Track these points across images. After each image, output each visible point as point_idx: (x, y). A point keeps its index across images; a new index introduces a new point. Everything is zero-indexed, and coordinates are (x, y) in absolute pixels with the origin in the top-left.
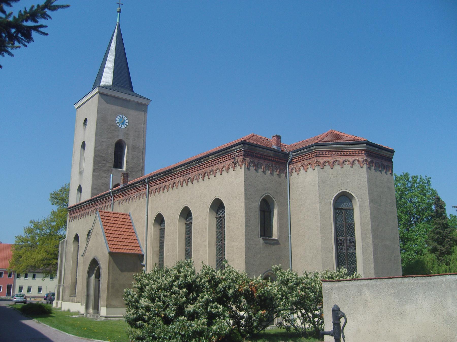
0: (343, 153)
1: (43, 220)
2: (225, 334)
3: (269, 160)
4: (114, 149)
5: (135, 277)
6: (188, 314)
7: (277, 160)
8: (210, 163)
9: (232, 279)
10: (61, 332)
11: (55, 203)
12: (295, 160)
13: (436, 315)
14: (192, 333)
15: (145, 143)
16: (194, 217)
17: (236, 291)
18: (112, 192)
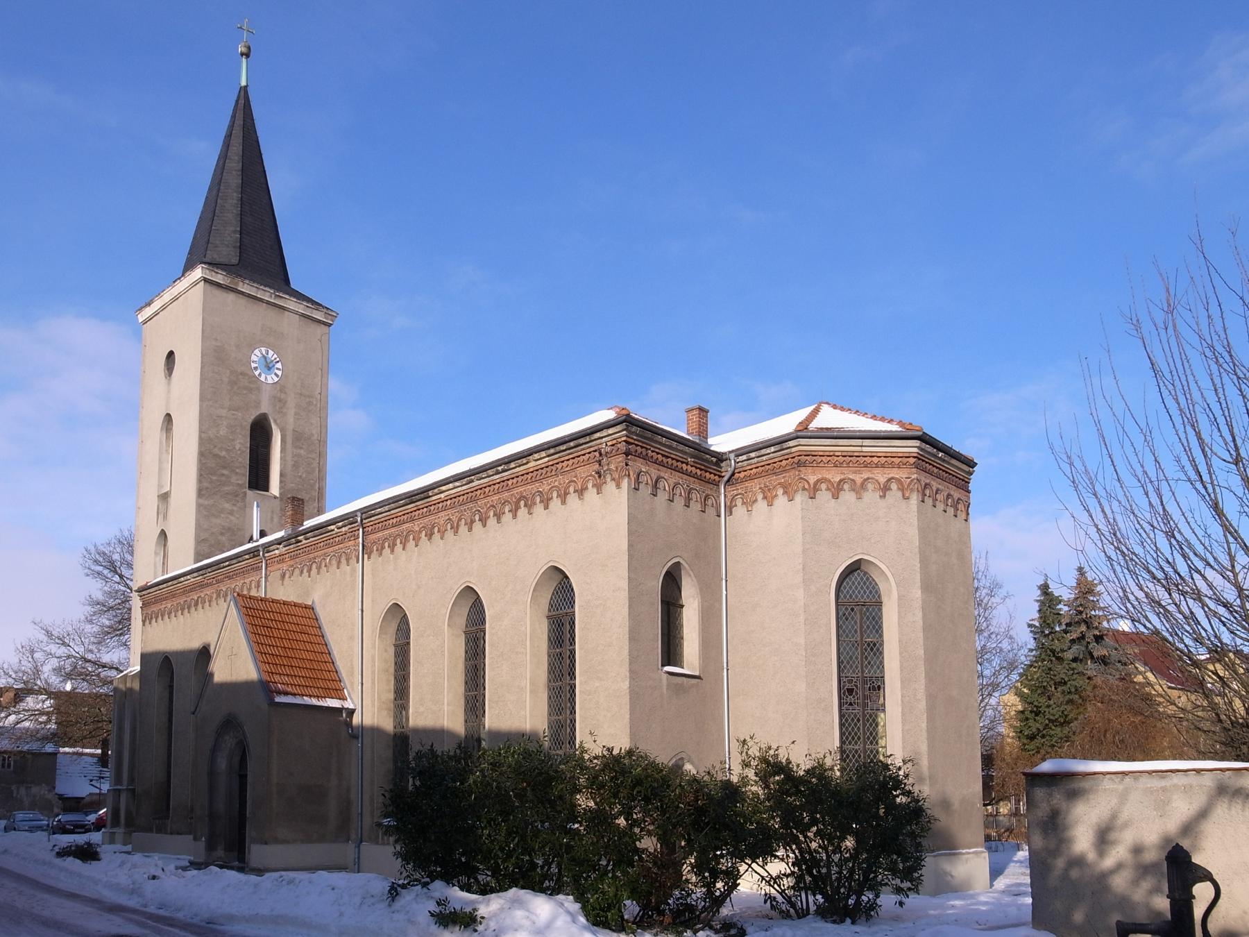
4: (249, 440)
7: (699, 472)
16: (489, 616)
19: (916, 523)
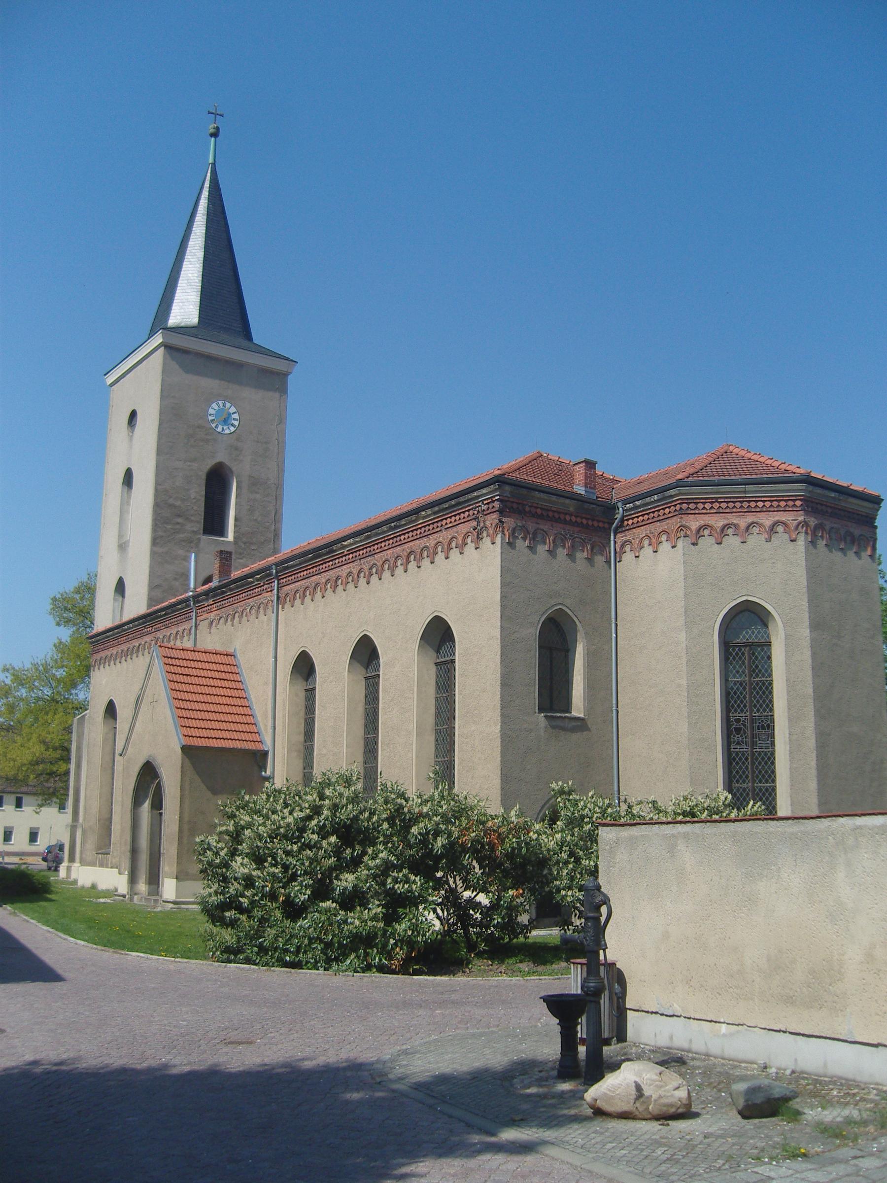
0: (747, 505)
1: (35, 665)
2: (425, 942)
3: (565, 522)
5: (222, 808)
6: (342, 894)
7: (585, 522)
8: (420, 528)
9: (443, 816)
10: (58, 935)
11: (64, 622)
12: (630, 522)
13: (814, 905)
14: (348, 940)
15: (281, 470)
17: (452, 844)
18: (194, 597)
19: (803, 563)
